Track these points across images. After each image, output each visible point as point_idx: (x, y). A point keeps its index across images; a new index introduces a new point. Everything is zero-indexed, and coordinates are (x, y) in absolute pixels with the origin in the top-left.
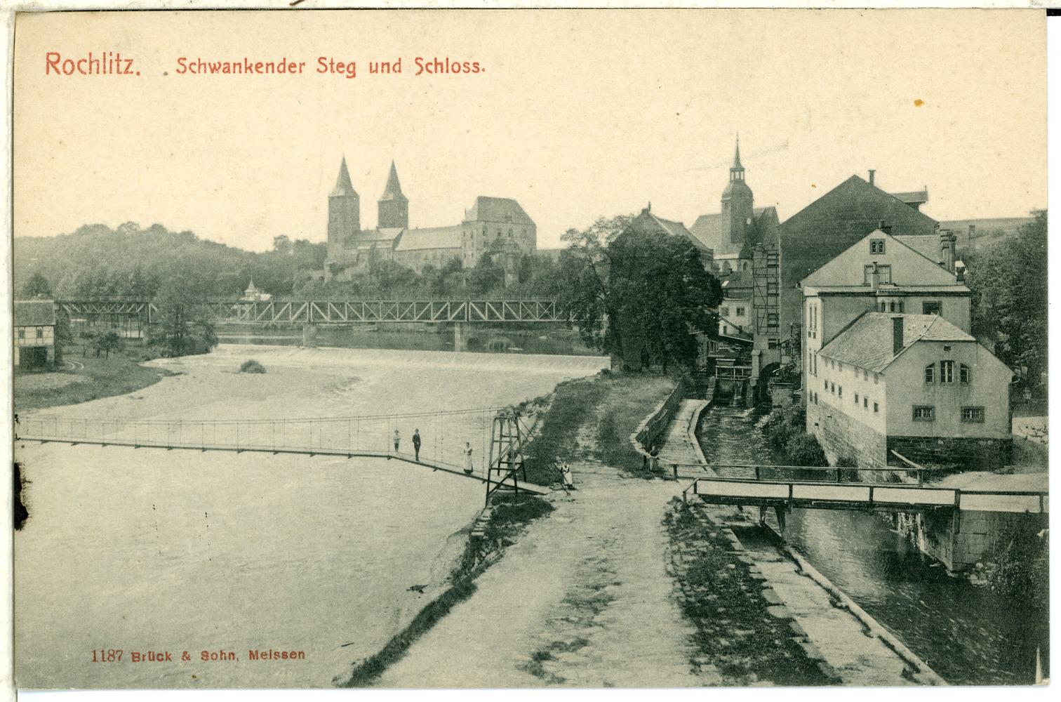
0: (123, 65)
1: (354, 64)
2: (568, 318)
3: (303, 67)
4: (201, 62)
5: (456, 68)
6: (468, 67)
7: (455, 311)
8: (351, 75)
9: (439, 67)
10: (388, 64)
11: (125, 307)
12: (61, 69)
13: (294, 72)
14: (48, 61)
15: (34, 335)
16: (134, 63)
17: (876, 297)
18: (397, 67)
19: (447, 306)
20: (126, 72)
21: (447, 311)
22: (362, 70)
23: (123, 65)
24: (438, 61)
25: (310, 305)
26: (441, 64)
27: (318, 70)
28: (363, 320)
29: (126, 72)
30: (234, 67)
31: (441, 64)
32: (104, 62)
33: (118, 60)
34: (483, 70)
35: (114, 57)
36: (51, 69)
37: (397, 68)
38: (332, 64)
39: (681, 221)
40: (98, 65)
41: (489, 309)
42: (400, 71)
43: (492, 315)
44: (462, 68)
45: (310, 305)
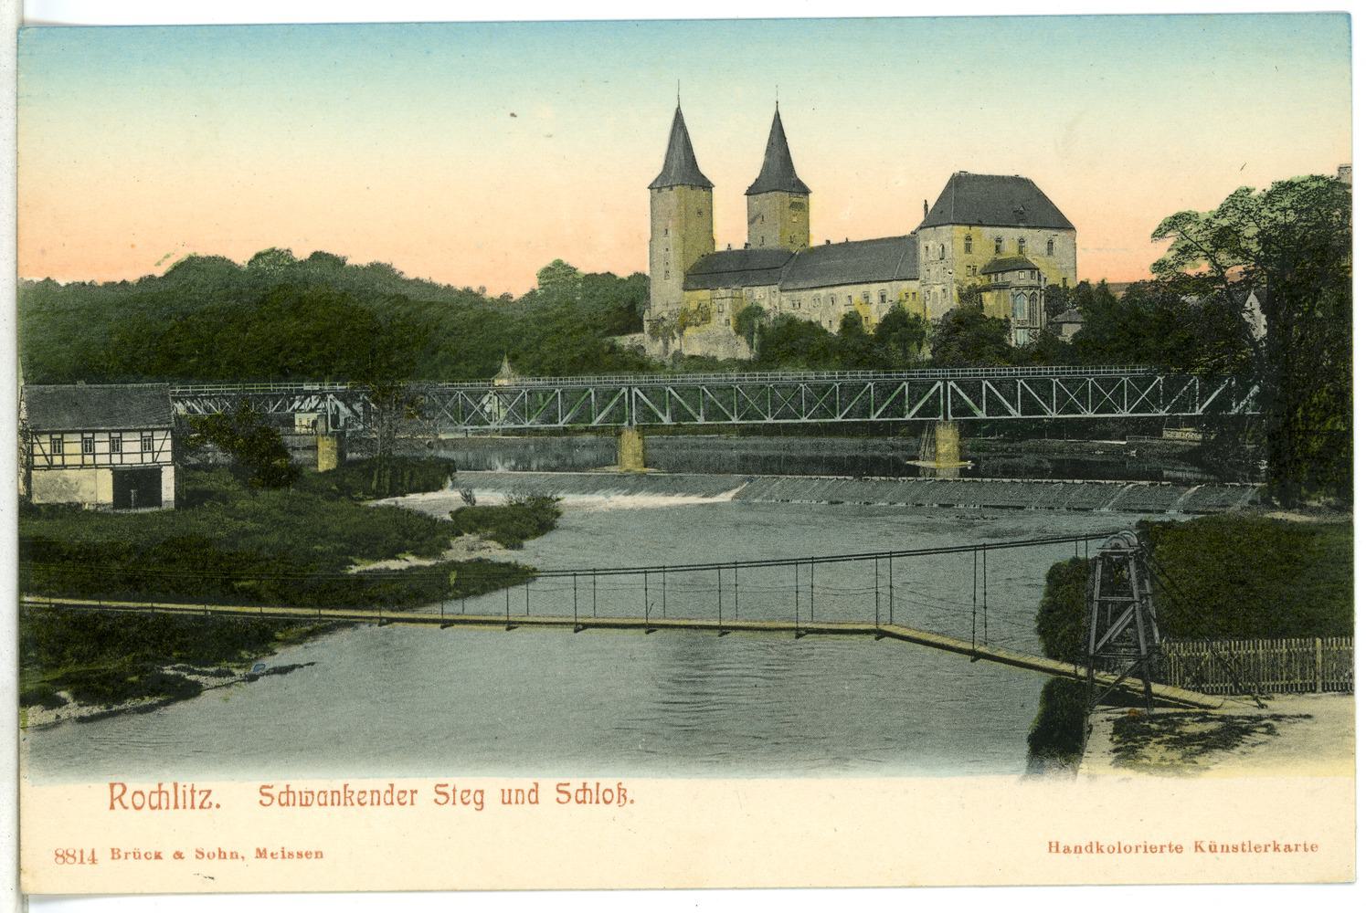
1: (482, 792)
3: (415, 795)
8: (479, 807)
13: (404, 804)
16: (213, 794)
19: (986, 385)
20: (201, 807)
21: (875, 405)
25: (630, 392)
27: (558, 800)
29: (201, 807)
30: (333, 795)
32: (597, 794)
33: (193, 791)
35: (188, 789)
36: (117, 803)
37: (533, 796)
39: (1350, 11)
40: (326, 797)
41: (1025, 394)
42: (537, 802)
43: (994, 406)
45: (630, 392)
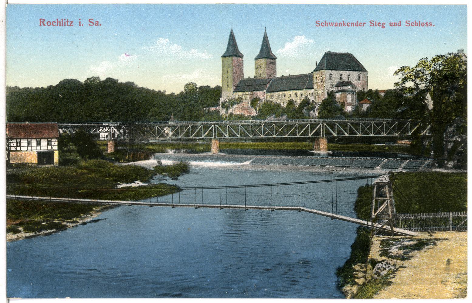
0: (69, 23)
2: (172, 146)
4: (326, 22)
5: (423, 24)
6: (372, 23)
7: (301, 132)
9: (59, 23)
10: (353, 23)
11: (96, 130)
12: (46, 24)
13: (349, 26)
14: (41, 22)
15: (46, 144)
17: (37, 146)
18: (400, 24)
20: (70, 25)
22: (387, 25)
23: (69, 23)
24: (326, 22)
26: (60, 22)
28: (251, 136)
31: (60, 22)
34: (434, 26)
35: (66, 20)
38: (376, 23)
44: (425, 25)
